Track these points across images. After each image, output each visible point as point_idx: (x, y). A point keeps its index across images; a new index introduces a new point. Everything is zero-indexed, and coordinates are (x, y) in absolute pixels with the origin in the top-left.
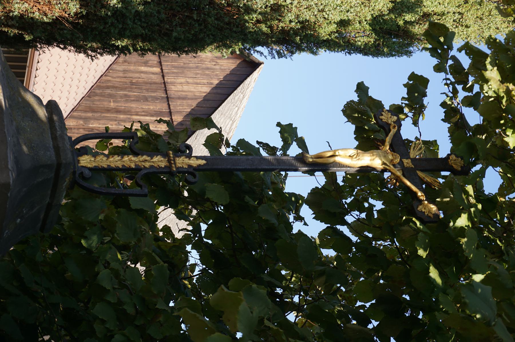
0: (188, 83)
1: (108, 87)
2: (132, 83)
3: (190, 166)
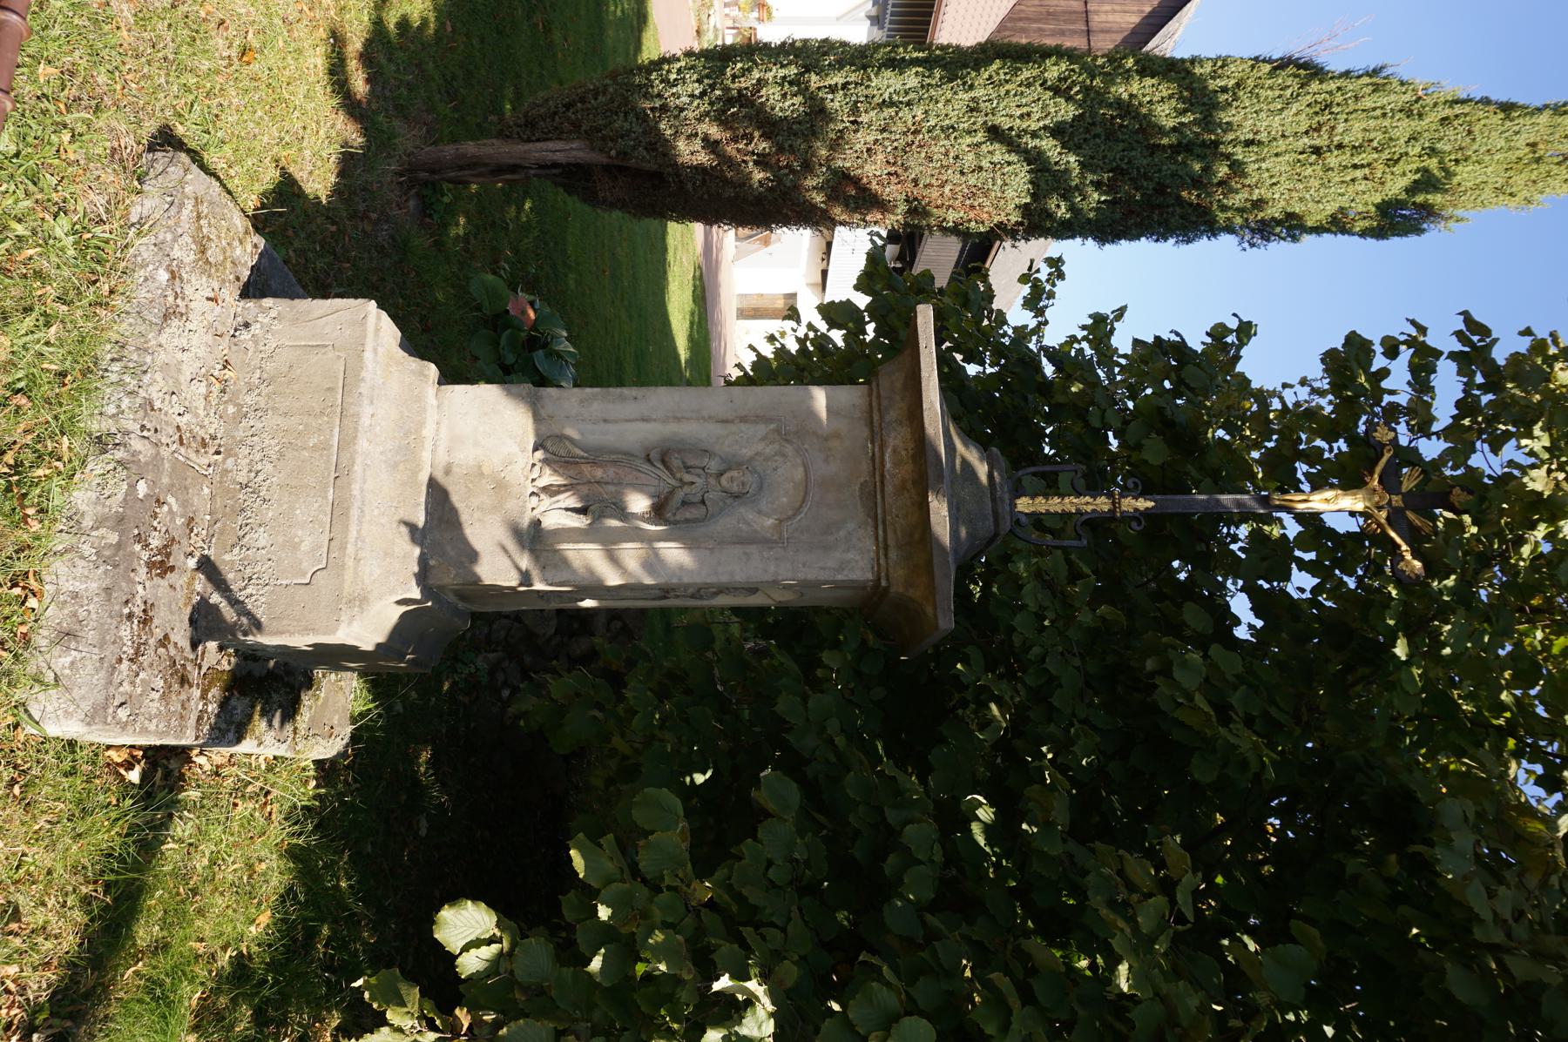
0: (1114, 11)
1: (1020, 19)
2: (1049, 14)
3: (1136, 510)
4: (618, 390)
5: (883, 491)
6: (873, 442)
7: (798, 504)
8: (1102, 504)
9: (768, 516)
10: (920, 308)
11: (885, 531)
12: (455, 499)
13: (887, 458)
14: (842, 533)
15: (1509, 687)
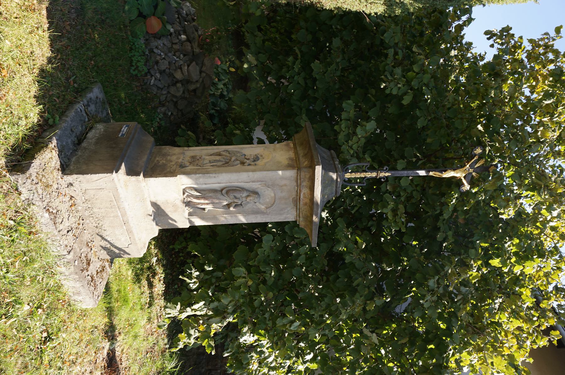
4: (208, 175)
5: (299, 203)
6: (297, 186)
7: (272, 203)
8: (374, 175)
9: (263, 205)
10: (317, 167)
11: (299, 211)
12: (163, 207)
13: (302, 195)
14: (286, 211)
15: (418, 365)
